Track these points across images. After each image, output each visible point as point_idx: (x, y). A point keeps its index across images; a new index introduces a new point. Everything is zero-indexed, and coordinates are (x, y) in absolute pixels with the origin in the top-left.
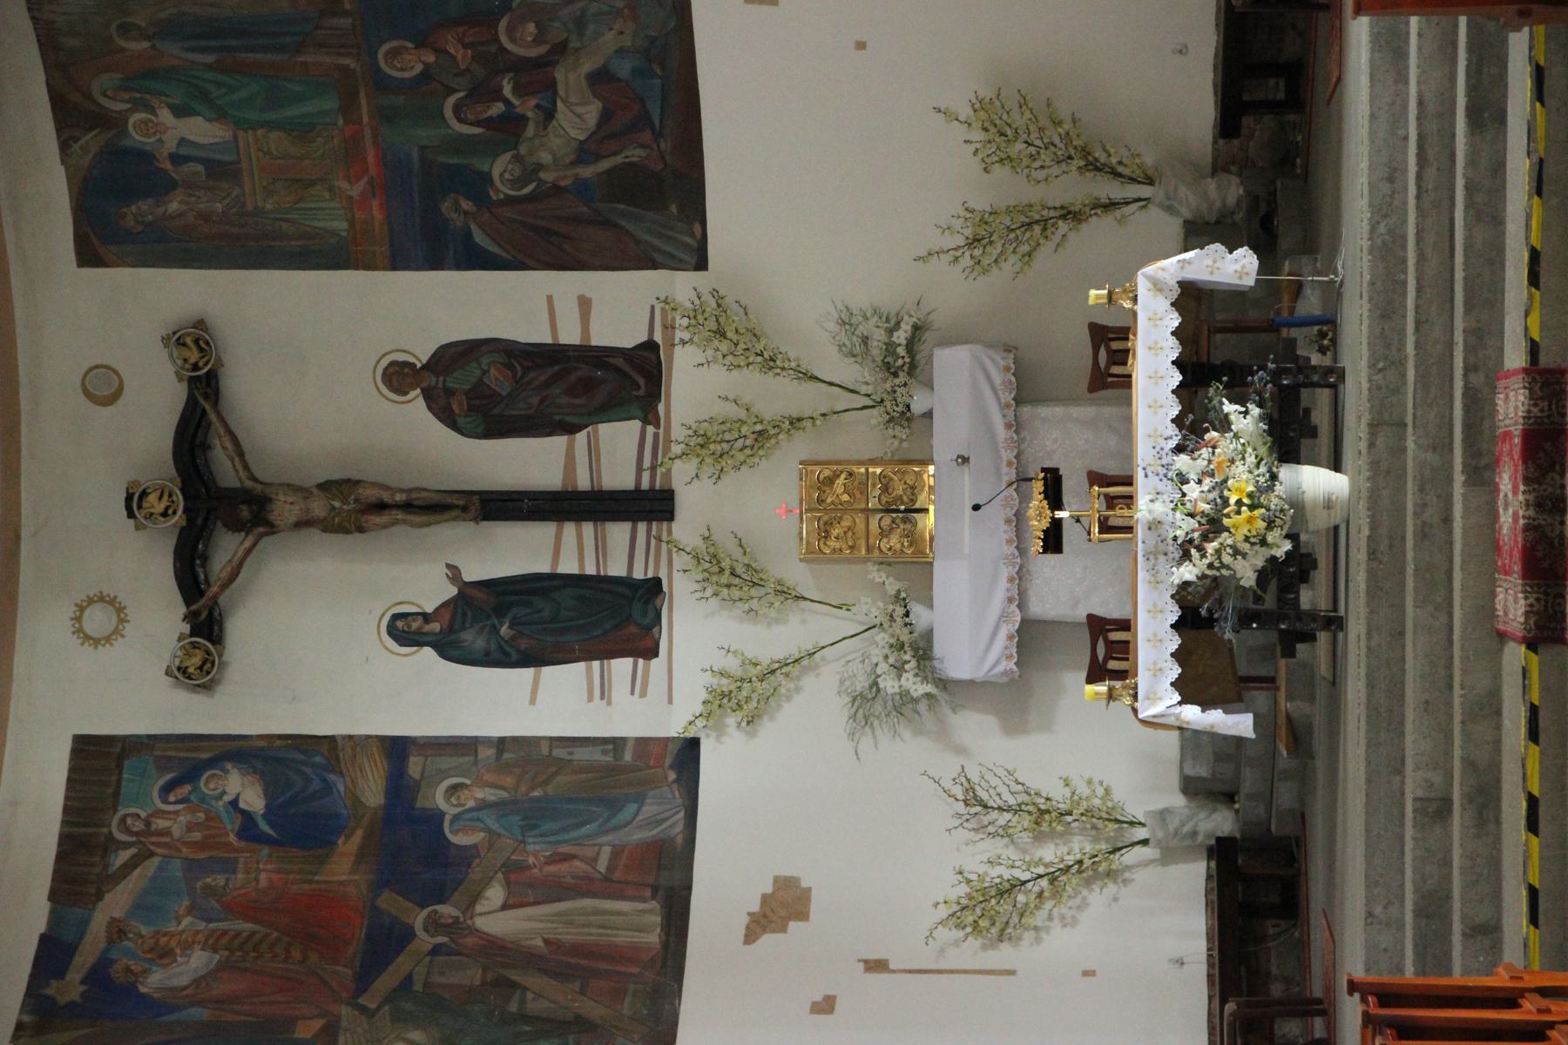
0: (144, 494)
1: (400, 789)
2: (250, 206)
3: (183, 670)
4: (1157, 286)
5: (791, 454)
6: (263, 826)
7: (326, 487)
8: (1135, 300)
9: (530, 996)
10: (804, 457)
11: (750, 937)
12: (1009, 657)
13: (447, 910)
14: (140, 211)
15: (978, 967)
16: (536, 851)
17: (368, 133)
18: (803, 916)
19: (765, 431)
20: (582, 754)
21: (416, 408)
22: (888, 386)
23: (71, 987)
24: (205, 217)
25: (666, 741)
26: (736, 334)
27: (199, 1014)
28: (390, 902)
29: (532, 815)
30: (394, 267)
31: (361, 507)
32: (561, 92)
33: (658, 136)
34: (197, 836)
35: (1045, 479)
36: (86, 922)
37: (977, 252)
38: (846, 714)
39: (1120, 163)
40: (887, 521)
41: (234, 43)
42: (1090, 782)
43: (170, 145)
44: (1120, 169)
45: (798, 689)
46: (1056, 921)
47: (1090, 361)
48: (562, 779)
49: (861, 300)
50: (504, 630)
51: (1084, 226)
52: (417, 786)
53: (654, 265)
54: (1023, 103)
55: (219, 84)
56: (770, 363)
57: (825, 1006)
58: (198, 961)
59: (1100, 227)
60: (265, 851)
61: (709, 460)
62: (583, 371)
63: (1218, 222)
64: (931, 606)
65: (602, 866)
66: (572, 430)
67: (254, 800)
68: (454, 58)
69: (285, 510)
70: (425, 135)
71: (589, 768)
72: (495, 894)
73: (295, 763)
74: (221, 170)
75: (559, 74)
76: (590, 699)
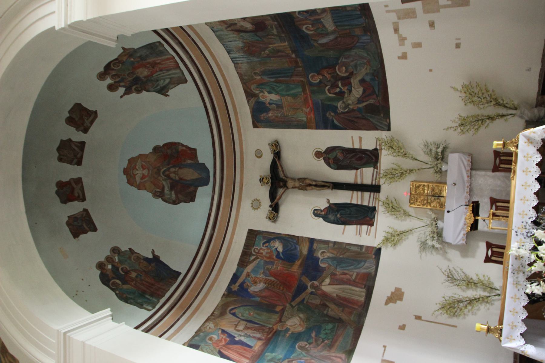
0: (263, 178)
1: (311, 251)
2: (285, 115)
3: (269, 218)
4: (530, 140)
5: (412, 177)
6: (281, 255)
7: (300, 179)
8: (517, 147)
9: (330, 310)
10: (413, 180)
11: (387, 303)
12: (463, 240)
13: (316, 283)
14: (264, 116)
15: (446, 323)
16: (339, 271)
17: (309, 97)
18: (401, 299)
19: (402, 173)
20: (353, 248)
21: (322, 161)
22: (436, 163)
23: (235, 287)
24: (277, 117)
25: (373, 248)
26: (396, 147)
27: (258, 299)
28: (304, 279)
29: (339, 261)
30: (317, 129)
31: (308, 184)
32: (353, 85)
33: (377, 96)
34: (268, 255)
35: (473, 206)
36: (243, 272)
37: (462, 128)
38: (419, 247)
39: (507, 103)
40: (433, 198)
41: (278, 75)
42: (484, 276)
43: (268, 101)
44: (507, 105)
45: (407, 238)
46: (470, 313)
47: (493, 164)
48: (347, 254)
49: (430, 140)
50: (338, 216)
51: (494, 122)
52: (315, 250)
53: (377, 129)
54: (478, 85)
55: (276, 86)
56: (405, 155)
57: (402, 327)
58: (261, 286)
59: (499, 122)
60: (281, 261)
61: (388, 179)
62: (360, 155)
63: (537, 121)
64: (443, 222)
65: (354, 277)
66: (357, 169)
67: (280, 249)
68: (326, 77)
69: (290, 184)
70: (322, 97)
71: (354, 252)
72: (328, 281)
73: (290, 241)
74: (279, 106)
75: (352, 81)
76: (356, 235)
